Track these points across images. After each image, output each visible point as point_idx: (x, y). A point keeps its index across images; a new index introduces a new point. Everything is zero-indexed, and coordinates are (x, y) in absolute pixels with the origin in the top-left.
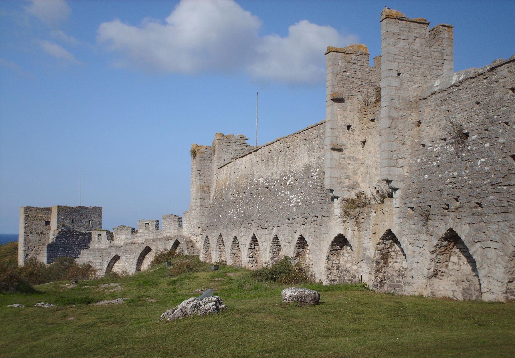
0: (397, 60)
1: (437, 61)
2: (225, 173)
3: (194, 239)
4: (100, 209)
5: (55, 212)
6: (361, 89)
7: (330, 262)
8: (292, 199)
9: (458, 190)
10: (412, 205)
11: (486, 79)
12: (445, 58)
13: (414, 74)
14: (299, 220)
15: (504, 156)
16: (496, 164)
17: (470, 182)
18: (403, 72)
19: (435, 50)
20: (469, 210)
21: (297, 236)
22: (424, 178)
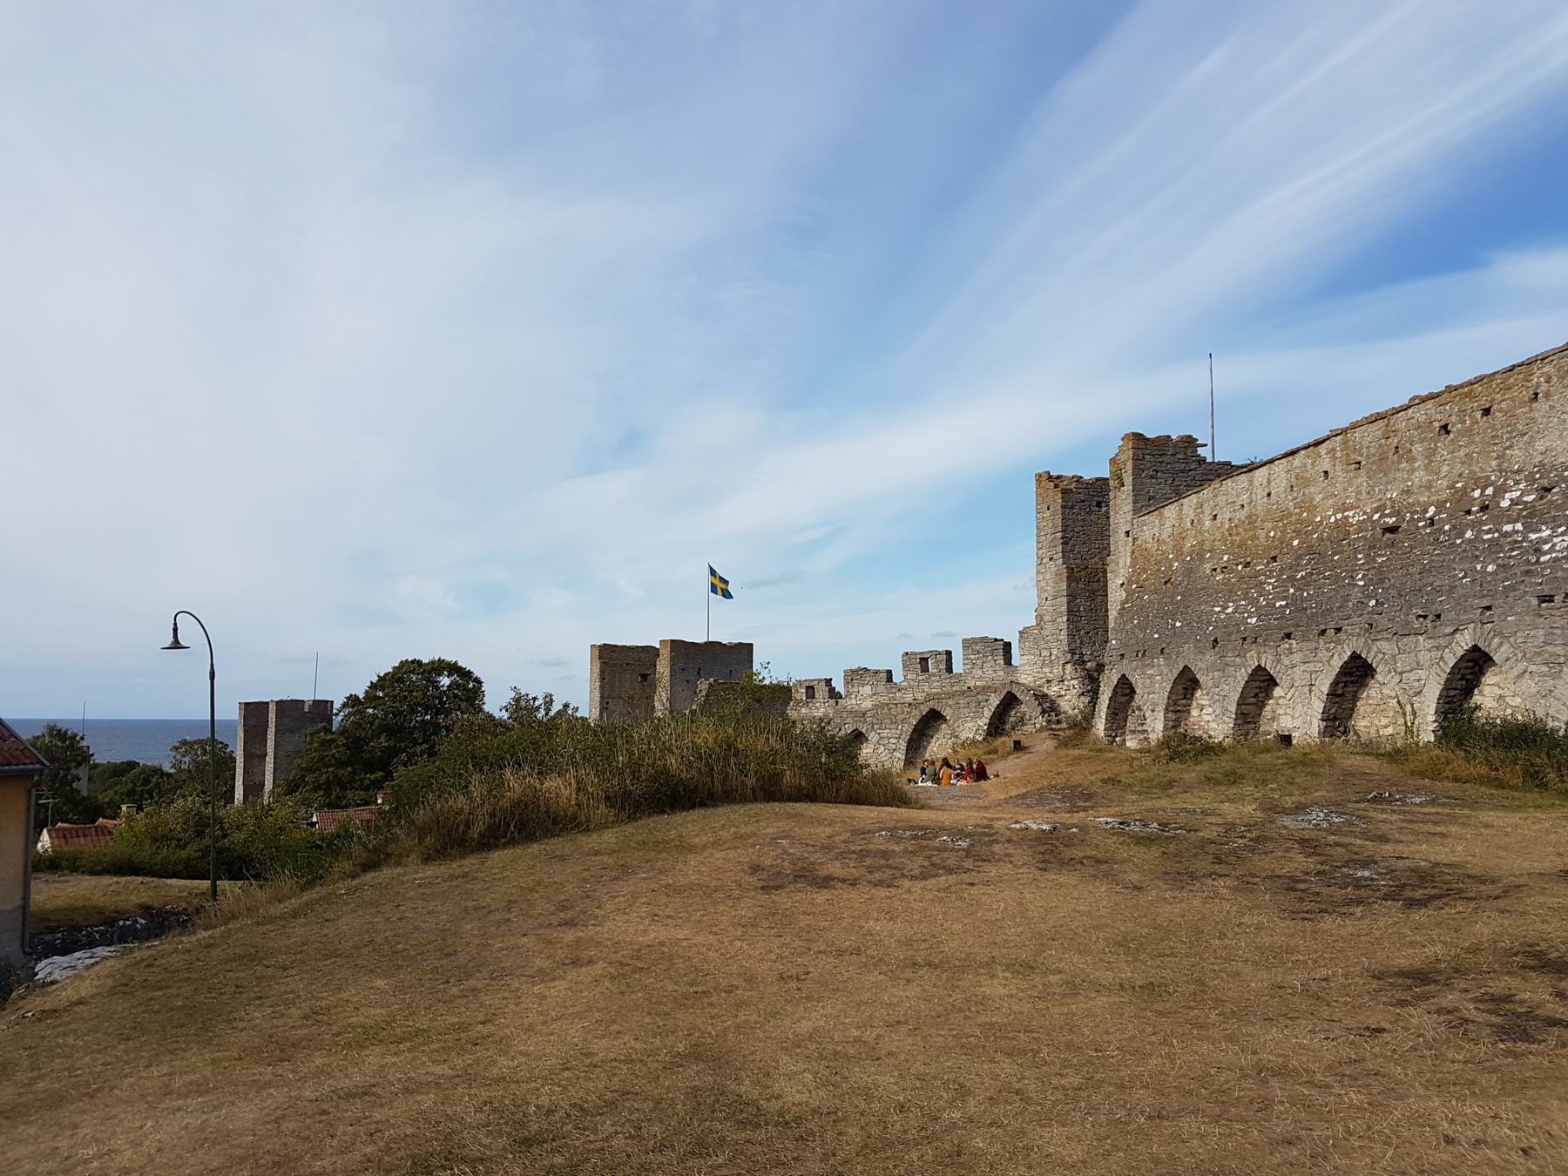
3: (1052, 691)
5: (665, 654)
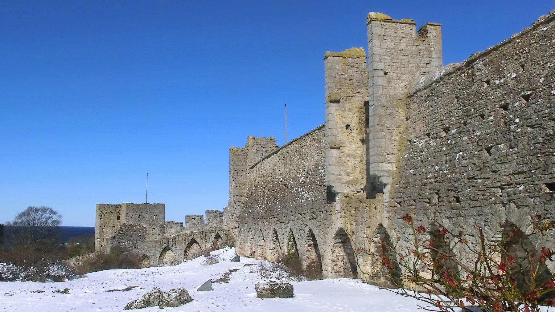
0: (383, 61)
1: (425, 59)
2: (255, 173)
4: (163, 205)
6: (359, 90)
7: (335, 255)
8: (303, 195)
9: (439, 184)
10: (399, 200)
11: (463, 73)
12: (434, 55)
13: (400, 72)
14: (308, 215)
15: (480, 149)
16: (473, 157)
17: (449, 176)
18: (390, 71)
19: (422, 48)
20: (448, 204)
21: (307, 229)
22: (410, 173)
